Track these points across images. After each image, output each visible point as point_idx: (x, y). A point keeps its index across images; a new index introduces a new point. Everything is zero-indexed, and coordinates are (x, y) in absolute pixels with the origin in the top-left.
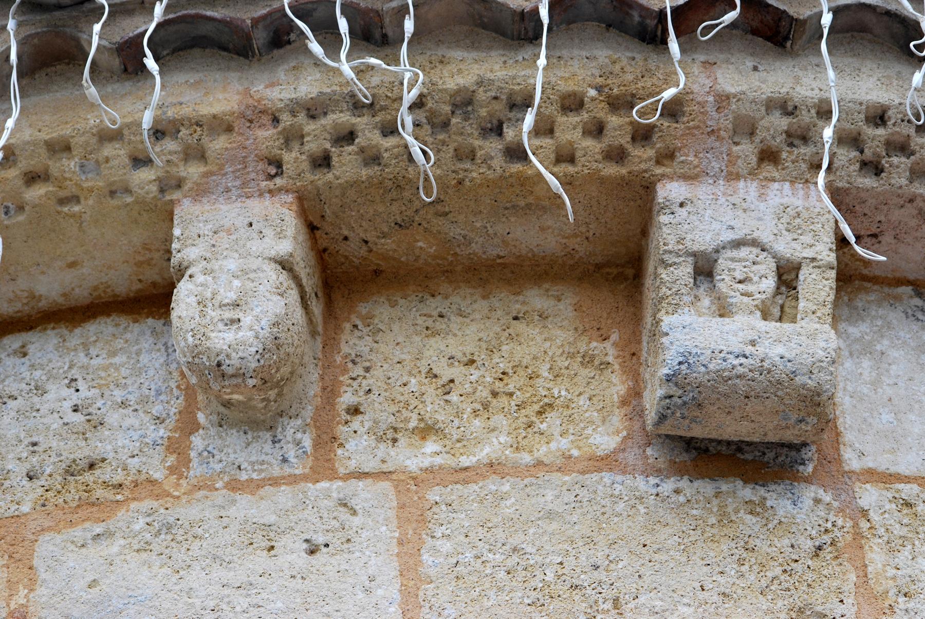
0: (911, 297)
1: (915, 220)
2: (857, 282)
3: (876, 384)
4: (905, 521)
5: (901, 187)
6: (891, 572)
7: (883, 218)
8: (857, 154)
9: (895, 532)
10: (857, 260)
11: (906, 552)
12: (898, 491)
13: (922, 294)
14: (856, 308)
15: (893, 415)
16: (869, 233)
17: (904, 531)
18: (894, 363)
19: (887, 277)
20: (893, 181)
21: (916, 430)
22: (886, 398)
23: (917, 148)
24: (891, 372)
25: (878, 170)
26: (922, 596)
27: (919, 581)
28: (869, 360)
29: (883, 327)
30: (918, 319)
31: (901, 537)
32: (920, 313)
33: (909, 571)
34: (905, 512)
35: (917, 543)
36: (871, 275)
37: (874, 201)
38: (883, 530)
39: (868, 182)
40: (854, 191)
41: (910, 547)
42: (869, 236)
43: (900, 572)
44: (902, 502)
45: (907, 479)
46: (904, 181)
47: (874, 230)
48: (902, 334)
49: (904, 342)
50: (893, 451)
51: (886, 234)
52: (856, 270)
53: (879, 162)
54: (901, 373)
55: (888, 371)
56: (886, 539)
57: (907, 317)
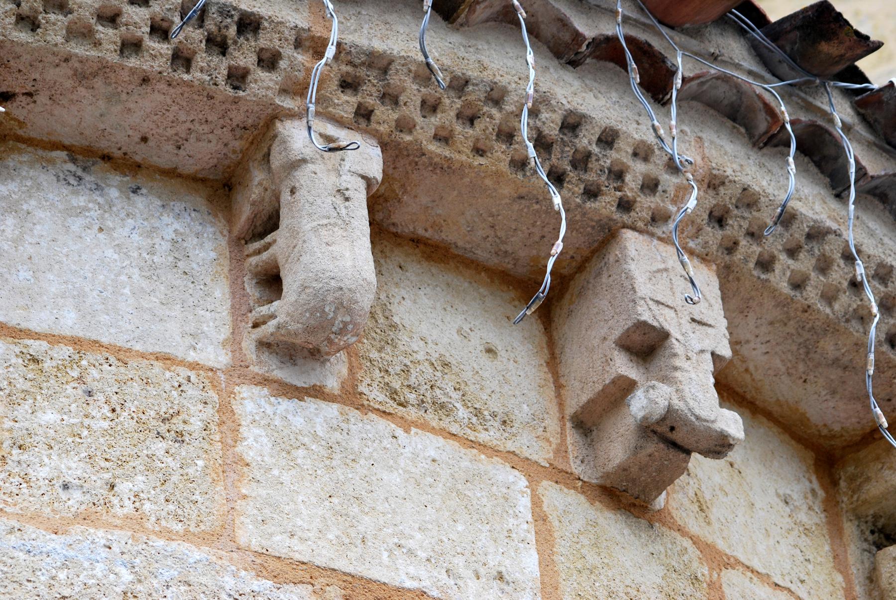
0: (65, 162)
1: (70, 81)
2: (11, 142)
3: (17, 241)
4: (30, 376)
5: (56, 45)
6: (8, 424)
7: (37, 76)
8: (14, 6)
9: (18, 386)
10: (12, 119)
11: (27, 406)
12: (26, 346)
13: (76, 160)
14: (7, 167)
15: (31, 273)
16: (24, 91)
17: (27, 385)
18: (39, 223)
19: (42, 140)
20: (49, 38)
21: (53, 290)
22: (26, 256)
23: (76, 7)
24: (35, 231)
25: (34, 26)
26: (36, 449)
27: (36, 434)
28: (14, 218)
29: (32, 187)
30: (69, 184)
31: (23, 391)
32: (73, 178)
33: (27, 424)
34: (31, 367)
35: (39, 397)
36: (26, 136)
37: (28, 56)
38: (6, 383)
39: (23, 36)
40: (8, 44)
41: (31, 401)
42: (24, 94)
43: (17, 425)
44: (29, 357)
45: (37, 336)
46: (59, 39)
47: (29, 88)
48: (51, 196)
49: (52, 205)
50: (26, 308)
51: (41, 93)
52: (11, 129)
53: (36, 18)
54: (44, 233)
55: (31, 230)
56: (7, 392)
57: (58, 180)
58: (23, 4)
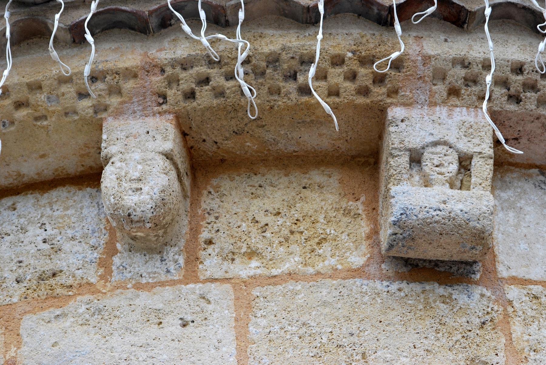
0: (538, 175)
1: (540, 130)
2: (506, 166)
3: (517, 226)
4: (534, 307)
5: (532, 110)
6: (526, 337)
7: (521, 129)
8: (506, 91)
9: (528, 314)
10: (506, 153)
11: (535, 326)
12: (530, 289)
13: (544, 173)
14: (505, 182)
15: (527, 245)
16: (513, 137)
17: (534, 313)
18: (528, 214)
19: (523, 164)
20: (527, 107)
21: (541, 254)
22: (523, 235)
23: (542, 87)
24: (526, 219)
25: (518, 100)
26: (544, 351)
27: (542, 342)
28: (513, 212)
29: (521, 193)
30: (542, 188)
31: (532, 317)
32: (543, 184)
33: (536, 337)
34: (534, 302)
35: (541, 320)
36: (514, 162)
37: (516, 118)
38: (521, 312)
39: (512, 107)
40: (504, 113)
41: (537, 323)
42: (513, 139)
43: (531, 337)
44: (532, 296)
45: (536, 283)
46: (533, 107)
47: (516, 136)
48: (532, 197)
49: (534, 202)
50: (527, 266)
51: (523, 138)
52: (505, 159)
53: (519, 96)
54: (532, 220)
55: (524, 219)
56: (523, 318)
57: (535, 187)
58: (511, 89)
